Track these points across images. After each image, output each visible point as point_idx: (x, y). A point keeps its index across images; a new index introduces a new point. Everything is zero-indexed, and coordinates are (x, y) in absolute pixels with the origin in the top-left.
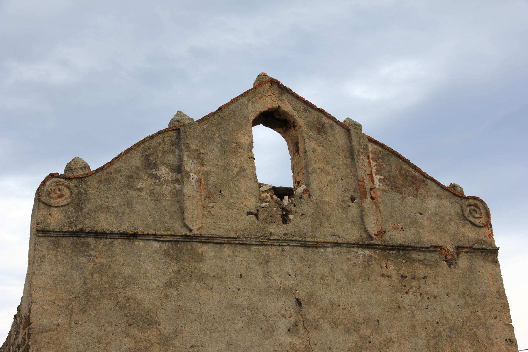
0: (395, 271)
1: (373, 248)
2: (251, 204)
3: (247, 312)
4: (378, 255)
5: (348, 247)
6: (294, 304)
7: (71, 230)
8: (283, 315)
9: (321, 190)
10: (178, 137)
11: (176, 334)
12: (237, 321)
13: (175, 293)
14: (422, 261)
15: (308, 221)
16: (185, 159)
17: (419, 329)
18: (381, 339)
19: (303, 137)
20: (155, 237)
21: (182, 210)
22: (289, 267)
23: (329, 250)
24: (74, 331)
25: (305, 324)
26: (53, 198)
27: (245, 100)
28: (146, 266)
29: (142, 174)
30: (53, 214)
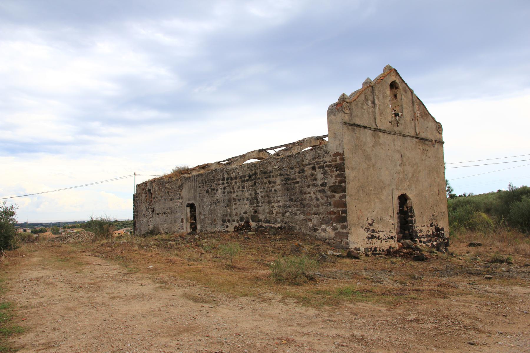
10: (373, 90)
11: (376, 163)
15: (403, 126)
16: (375, 99)
17: (426, 167)
20: (370, 128)
21: (375, 119)
23: (408, 138)
29: (365, 103)
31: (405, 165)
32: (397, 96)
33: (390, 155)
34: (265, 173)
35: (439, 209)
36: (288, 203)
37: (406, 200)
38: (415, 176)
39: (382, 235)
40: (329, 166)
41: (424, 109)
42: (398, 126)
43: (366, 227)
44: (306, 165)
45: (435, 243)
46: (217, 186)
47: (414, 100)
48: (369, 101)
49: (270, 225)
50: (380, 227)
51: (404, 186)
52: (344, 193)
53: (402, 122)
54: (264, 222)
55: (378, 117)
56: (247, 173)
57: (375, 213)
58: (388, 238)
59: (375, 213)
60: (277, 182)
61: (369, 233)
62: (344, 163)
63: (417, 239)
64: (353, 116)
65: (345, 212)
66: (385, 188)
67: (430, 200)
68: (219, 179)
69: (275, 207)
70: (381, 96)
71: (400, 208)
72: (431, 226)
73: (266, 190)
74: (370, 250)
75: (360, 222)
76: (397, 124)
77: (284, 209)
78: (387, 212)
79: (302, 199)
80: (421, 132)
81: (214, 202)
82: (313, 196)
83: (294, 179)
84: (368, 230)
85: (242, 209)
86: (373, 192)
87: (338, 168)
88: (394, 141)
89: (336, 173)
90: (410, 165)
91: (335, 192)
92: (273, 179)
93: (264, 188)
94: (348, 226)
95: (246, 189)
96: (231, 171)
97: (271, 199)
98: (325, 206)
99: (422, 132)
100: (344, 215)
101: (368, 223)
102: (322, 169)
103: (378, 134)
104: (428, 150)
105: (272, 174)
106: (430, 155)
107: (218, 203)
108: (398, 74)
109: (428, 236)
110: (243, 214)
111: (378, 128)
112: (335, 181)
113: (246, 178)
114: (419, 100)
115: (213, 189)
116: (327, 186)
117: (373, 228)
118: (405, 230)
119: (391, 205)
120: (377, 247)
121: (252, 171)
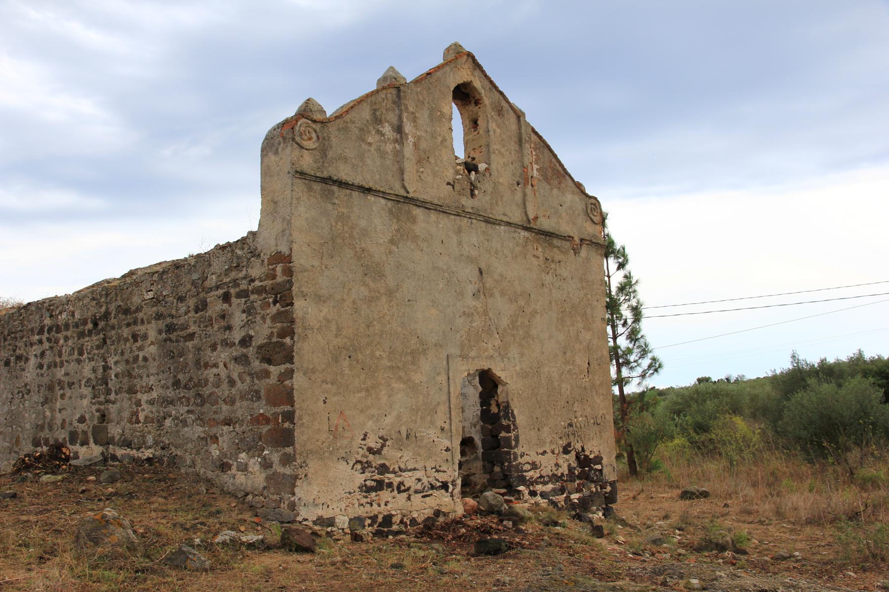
0: (542, 254)
1: (531, 231)
2: (450, 175)
3: (447, 275)
4: (533, 237)
5: (515, 227)
6: (477, 272)
7: (322, 176)
8: (470, 282)
9: (498, 171)
10: (399, 96)
12: (439, 283)
13: (396, 250)
14: (559, 247)
15: (488, 198)
16: (405, 120)
17: (553, 304)
18: (530, 310)
19: (487, 116)
20: (383, 195)
21: (402, 172)
22: (475, 239)
23: (502, 228)
24: (325, 274)
25: (485, 291)
26: (303, 139)
27: (447, 69)
28: (376, 221)
29: (371, 128)
30: (305, 156)
31: (492, 295)
32: (479, 122)
33: (445, 267)
34: (127, 312)
35: (589, 409)
36: (170, 393)
37: (496, 386)
38: (519, 323)
39: (413, 479)
40: (259, 291)
41: (554, 160)
42: (473, 195)
43: (359, 458)
44: (211, 289)
45: (575, 497)
46: (26, 348)
47: (524, 136)
48: (387, 124)
49: (131, 453)
50: (404, 459)
51: (487, 349)
52: (288, 365)
53: (486, 185)
54: (118, 445)
55: (410, 167)
56: (90, 314)
57: (389, 420)
58: (433, 487)
59: (389, 420)
60: (150, 335)
61: (371, 474)
62: (290, 283)
63: (521, 488)
64: (329, 157)
65: (289, 416)
66: (425, 354)
67: (564, 385)
68: (32, 330)
69: (142, 403)
70: (424, 117)
71: (481, 406)
72: (566, 451)
73: (126, 357)
74: (369, 521)
75: (339, 445)
76: (472, 191)
77: (161, 409)
78: (429, 418)
79: (199, 382)
80: (540, 214)
81: (19, 393)
82: (223, 373)
83: (184, 327)
84: (365, 466)
85: (75, 408)
86: (386, 362)
87: (279, 296)
88: (460, 232)
89: (274, 309)
90: (507, 297)
91: (269, 362)
92: (141, 329)
93: (122, 353)
94: (298, 457)
95: (86, 355)
96: (57, 307)
97: (135, 381)
98: (247, 400)
99: (544, 216)
100: (286, 425)
101: (365, 448)
102: (243, 300)
103: (409, 212)
104: (560, 262)
105: (140, 315)
106: (565, 273)
107: (28, 394)
108: (477, 66)
109: (554, 478)
110: (76, 424)
111: (410, 195)
112: (270, 330)
113: (86, 328)
114: (540, 137)
115: (19, 358)
116: (254, 344)
117: (382, 462)
118: (494, 465)
119: (444, 397)
120: (393, 513)
121: (101, 307)
